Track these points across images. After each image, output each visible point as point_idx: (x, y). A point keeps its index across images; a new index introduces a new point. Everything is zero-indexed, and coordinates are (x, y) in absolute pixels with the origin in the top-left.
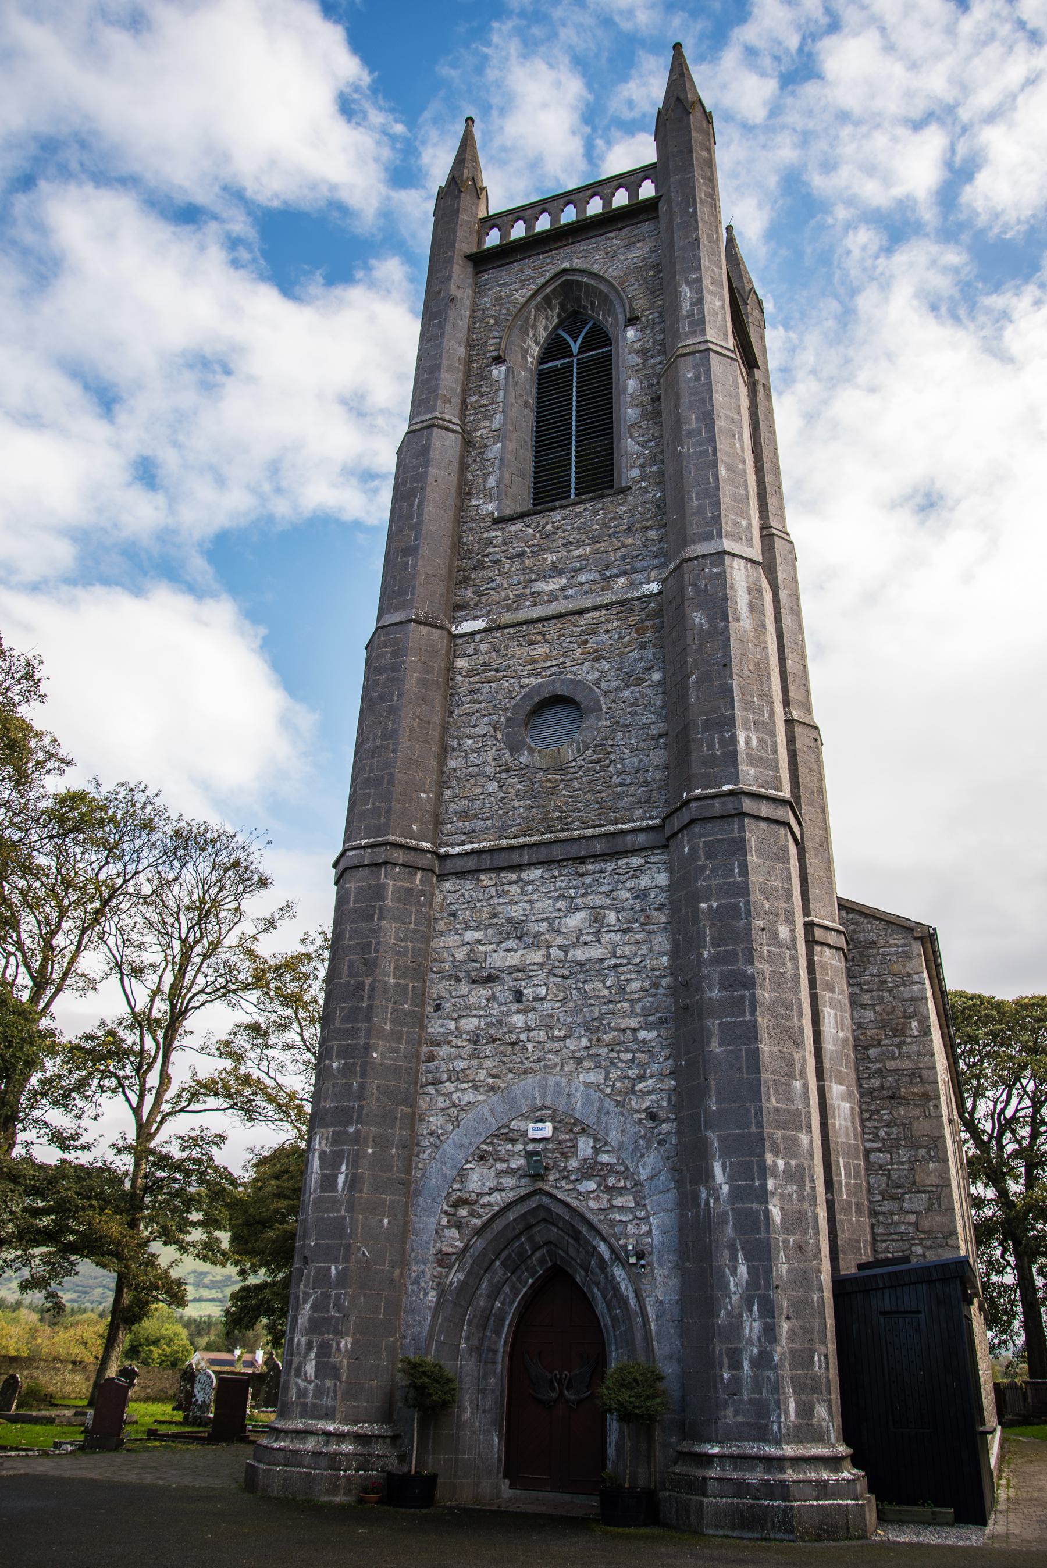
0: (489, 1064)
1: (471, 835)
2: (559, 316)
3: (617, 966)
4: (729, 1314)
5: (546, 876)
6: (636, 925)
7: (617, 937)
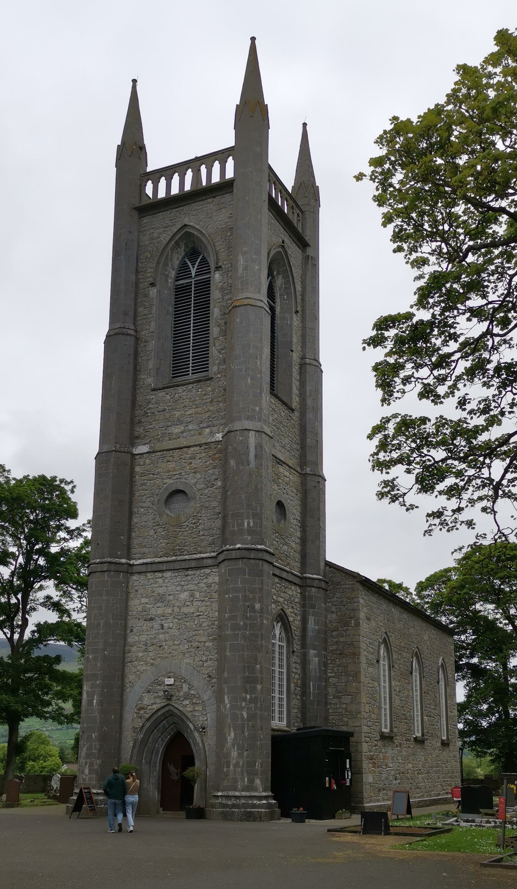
0: (151, 654)
1: (143, 557)
2: (185, 250)
3: (199, 615)
4: (227, 749)
5: (173, 575)
6: (207, 599)
7: (199, 603)
